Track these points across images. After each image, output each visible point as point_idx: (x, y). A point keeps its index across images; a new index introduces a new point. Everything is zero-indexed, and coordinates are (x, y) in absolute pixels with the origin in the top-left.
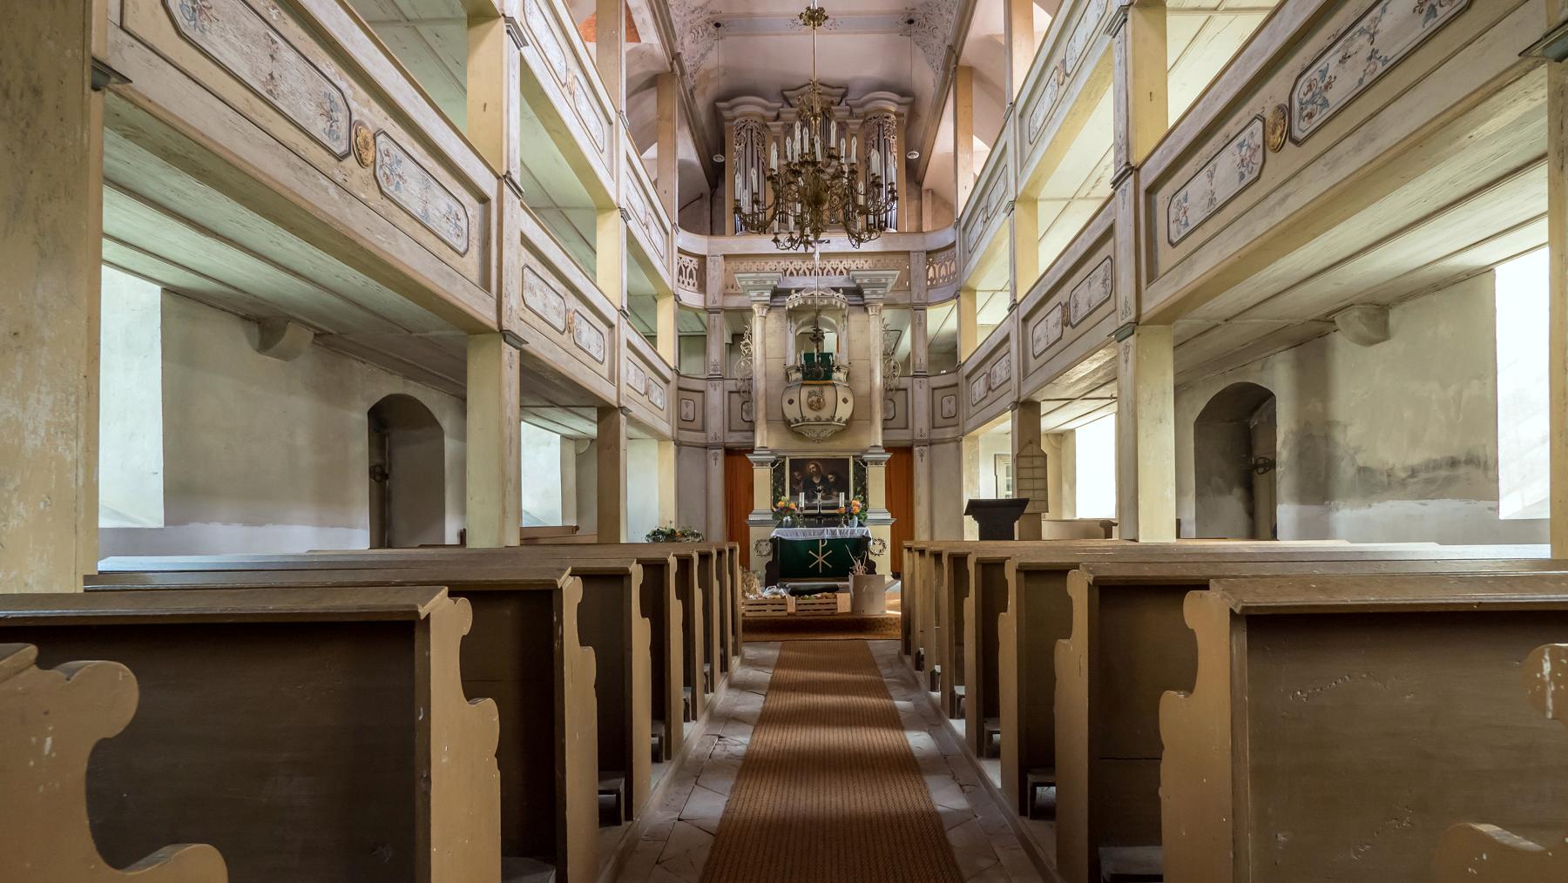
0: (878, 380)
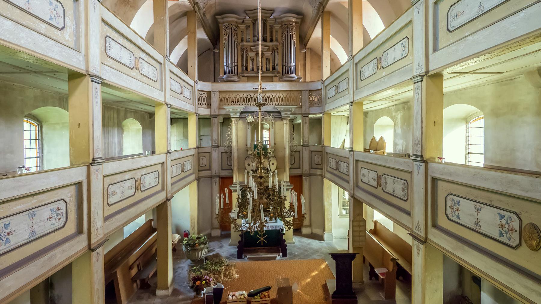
0: (287, 152)
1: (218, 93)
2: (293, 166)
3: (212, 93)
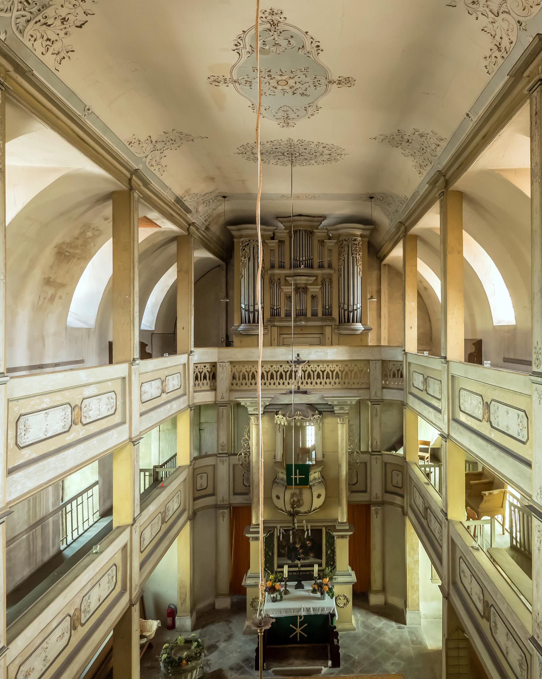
1: (228, 365)
2: (355, 488)
3: (218, 364)
